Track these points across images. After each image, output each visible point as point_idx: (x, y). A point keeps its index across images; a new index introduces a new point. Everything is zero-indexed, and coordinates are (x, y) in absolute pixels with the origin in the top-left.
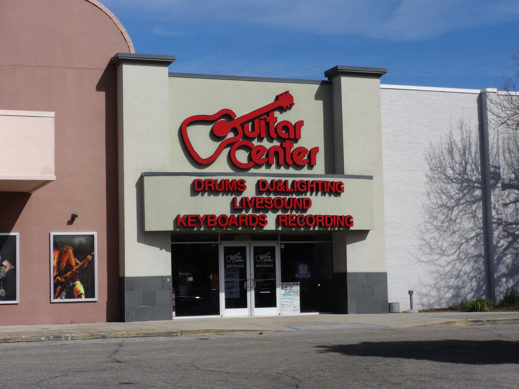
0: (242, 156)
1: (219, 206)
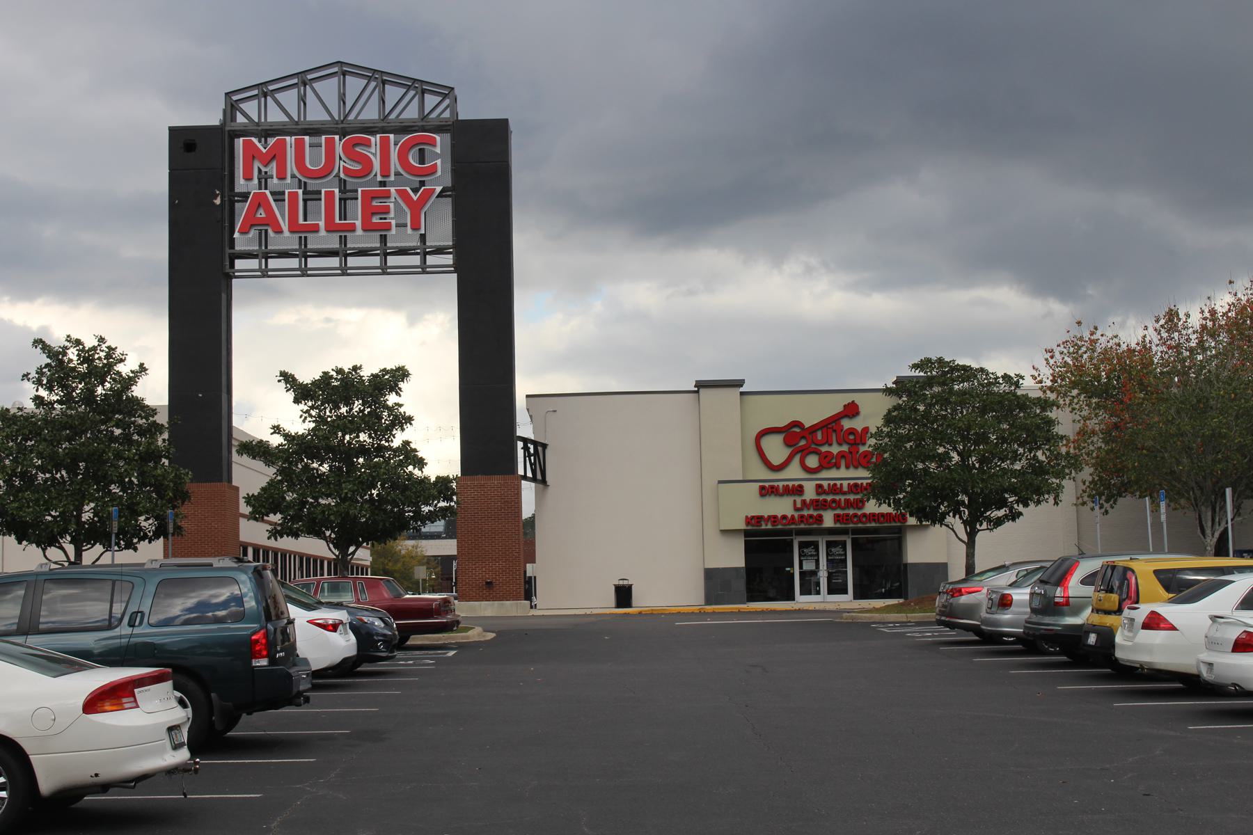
0: (812, 461)
1: (782, 507)
